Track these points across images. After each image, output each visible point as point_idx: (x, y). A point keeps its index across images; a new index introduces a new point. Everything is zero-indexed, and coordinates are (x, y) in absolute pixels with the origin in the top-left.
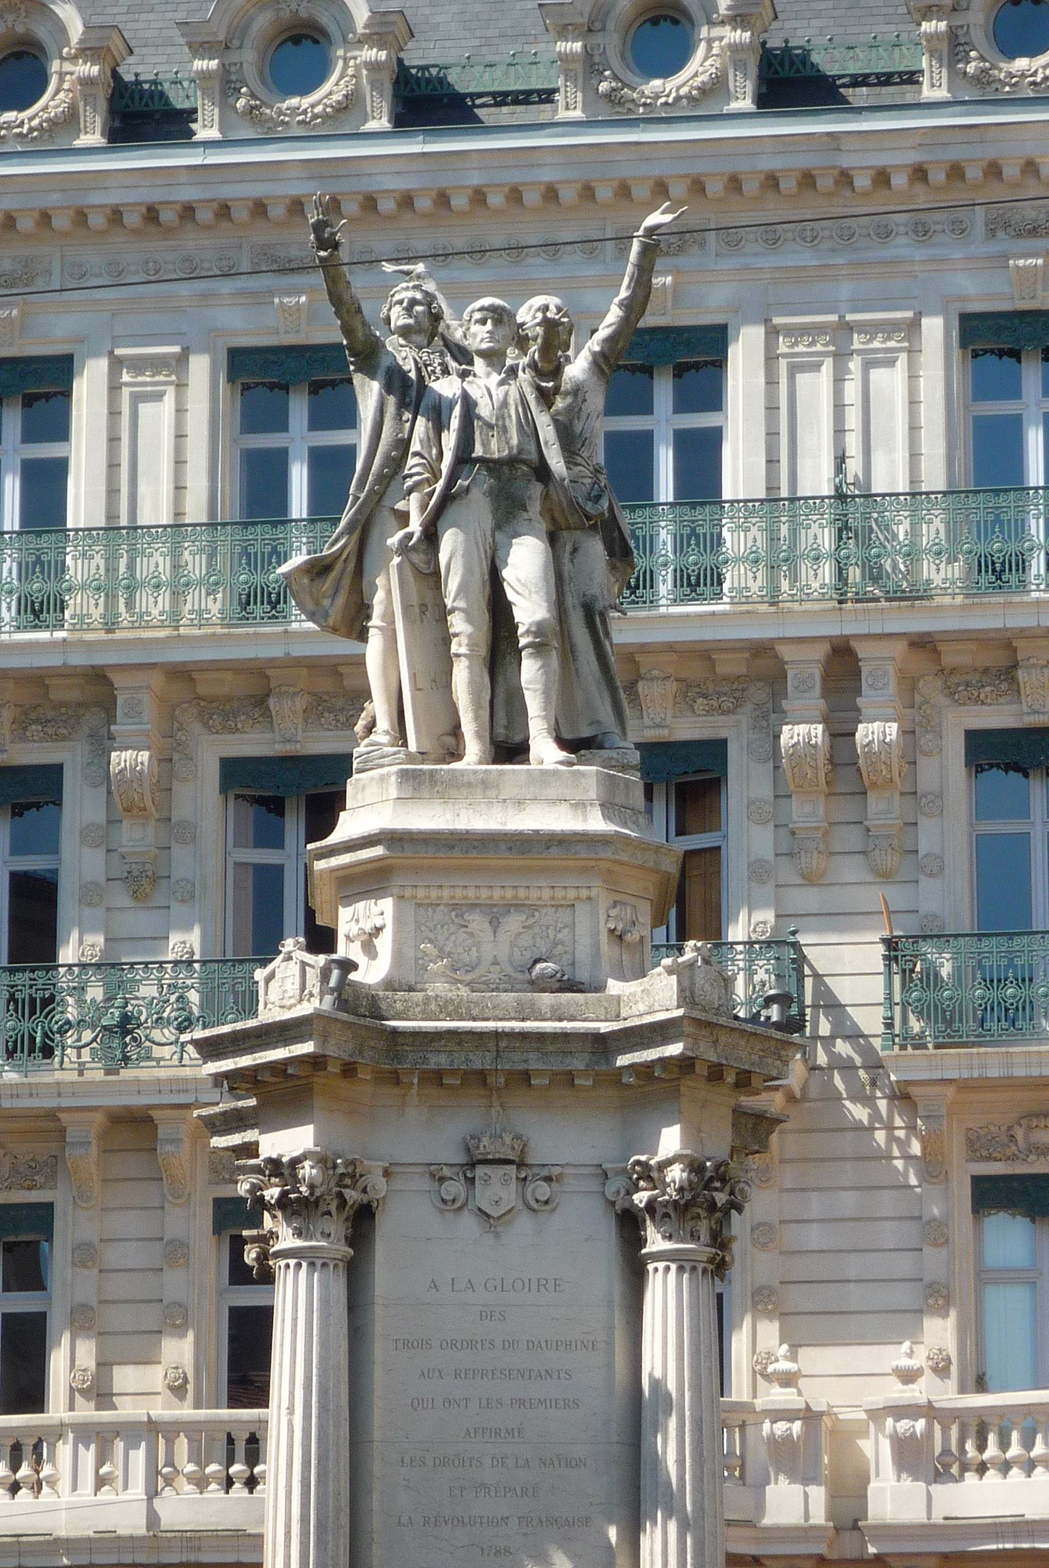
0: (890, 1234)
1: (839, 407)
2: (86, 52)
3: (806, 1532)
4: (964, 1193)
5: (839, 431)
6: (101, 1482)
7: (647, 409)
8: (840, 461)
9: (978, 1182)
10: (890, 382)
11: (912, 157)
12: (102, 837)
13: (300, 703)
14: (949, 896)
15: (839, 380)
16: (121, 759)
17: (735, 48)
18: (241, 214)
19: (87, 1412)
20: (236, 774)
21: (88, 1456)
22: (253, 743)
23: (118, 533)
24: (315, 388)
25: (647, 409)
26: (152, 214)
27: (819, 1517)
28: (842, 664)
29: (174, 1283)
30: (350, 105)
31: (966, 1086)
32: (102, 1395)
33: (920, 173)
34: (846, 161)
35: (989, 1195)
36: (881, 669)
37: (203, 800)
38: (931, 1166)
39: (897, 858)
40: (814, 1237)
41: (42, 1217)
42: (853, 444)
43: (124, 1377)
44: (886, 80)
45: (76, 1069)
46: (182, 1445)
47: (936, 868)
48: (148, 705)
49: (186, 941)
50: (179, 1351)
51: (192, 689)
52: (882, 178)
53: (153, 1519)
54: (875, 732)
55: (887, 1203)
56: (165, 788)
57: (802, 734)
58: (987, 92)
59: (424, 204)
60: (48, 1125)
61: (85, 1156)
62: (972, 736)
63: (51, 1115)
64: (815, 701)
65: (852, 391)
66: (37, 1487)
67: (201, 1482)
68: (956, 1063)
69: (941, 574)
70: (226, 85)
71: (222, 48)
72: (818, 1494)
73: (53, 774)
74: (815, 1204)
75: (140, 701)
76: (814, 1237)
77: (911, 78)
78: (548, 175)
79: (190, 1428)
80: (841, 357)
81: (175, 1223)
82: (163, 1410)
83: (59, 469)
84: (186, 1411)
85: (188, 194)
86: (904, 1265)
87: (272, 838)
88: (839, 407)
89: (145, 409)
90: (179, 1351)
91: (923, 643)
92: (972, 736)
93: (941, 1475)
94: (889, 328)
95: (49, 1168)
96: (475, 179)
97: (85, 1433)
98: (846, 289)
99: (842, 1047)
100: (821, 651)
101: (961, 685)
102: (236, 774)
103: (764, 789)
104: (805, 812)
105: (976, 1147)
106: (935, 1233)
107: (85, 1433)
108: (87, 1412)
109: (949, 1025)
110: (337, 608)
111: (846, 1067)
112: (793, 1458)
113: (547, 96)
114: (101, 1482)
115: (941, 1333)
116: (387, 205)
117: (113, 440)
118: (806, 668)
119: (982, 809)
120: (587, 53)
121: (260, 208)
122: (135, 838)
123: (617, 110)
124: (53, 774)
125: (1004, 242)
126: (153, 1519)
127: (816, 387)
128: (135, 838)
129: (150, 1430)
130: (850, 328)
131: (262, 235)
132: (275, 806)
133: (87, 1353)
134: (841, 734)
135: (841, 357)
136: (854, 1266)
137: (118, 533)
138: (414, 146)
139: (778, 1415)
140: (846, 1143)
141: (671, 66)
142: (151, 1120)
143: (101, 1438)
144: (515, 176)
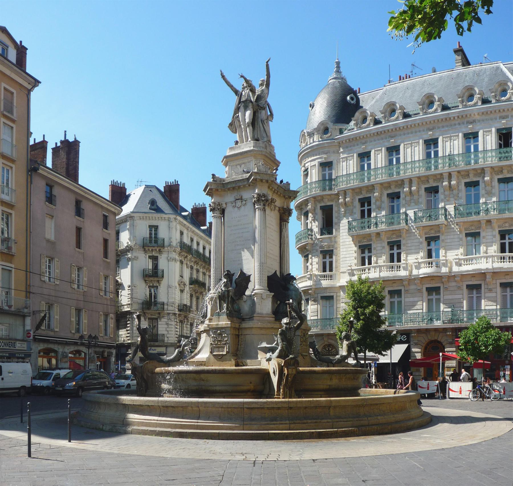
0: (456, 240)
1: (450, 146)
2: (439, 101)
3: (446, 273)
4: (464, 235)
5: (450, 149)
6: (487, 262)
7: (431, 149)
8: (412, 158)
9: (388, 242)
10: (456, 142)
11: (457, 115)
12: (375, 204)
13: (394, 186)
14: (463, 201)
15: (450, 143)
16: (486, 179)
17: (438, 105)
18: (386, 132)
19: (485, 255)
20: (389, 195)
21: (485, 259)
22: (390, 191)
23: (485, 151)
24: (396, 151)
25: (431, 149)
26: (446, 119)
27: (447, 271)
28: (450, 175)
29: (383, 251)
30: (398, 117)
31: (464, 222)
32: (486, 252)
33: (458, 117)
34: (450, 116)
35: (467, 235)
36: (454, 175)
37: (385, 198)
38: (461, 232)
39: (457, 197)
40: (448, 241)
41: (371, 245)
42: (452, 150)
43: (379, 261)
44: (456, 107)
45: (373, 228)
46: (496, 258)
47: (461, 198)
48: (455, 177)
49: (384, 213)
50: (384, 258)
51: (385, 185)
52: (454, 118)
53: (380, 275)
54: (453, 182)
55: (456, 236)
56: (381, 197)
57: (406, 189)
58: (466, 106)
59: (405, 127)
60: (369, 235)
61: (483, 225)
62: (465, 183)
63: (370, 234)
64: (447, 180)
65: (452, 144)
66: (504, 262)
67: (387, 271)
68: (462, 220)
69: (462, 164)
70: (385, 117)
71: (423, 105)
72: (447, 268)
73: (478, 182)
74: (449, 237)
75: (488, 171)
76: (448, 241)
77: (458, 106)
78: (418, 122)
79: (386, 266)
80: (451, 140)
81: (494, 233)
82: (494, 254)
83: (438, 151)
84: (496, 254)
85: (381, 130)
86: (458, 243)
87: (393, 202)
88: (450, 146)
89: (487, 137)
90: (384, 258)
91: (459, 172)
92: (465, 183)
93: (460, 265)
94: (456, 136)
95: (480, 228)
96: (410, 123)
97: (484, 257)
98: (451, 132)
99: (451, 219)
100: (408, 180)
101: (464, 177)
102: (389, 195)
103: (484, 186)
104: (447, 193)
105: (466, 229)
106: (461, 239)
107: (484, 257)
108: (485, 255)
109: (461, 215)
111: (452, 221)
112: (445, 265)
113: (419, 114)
114: (487, 262)
115: (461, 250)
116: (401, 128)
117: (375, 160)
118: (446, 176)
119: (467, 191)
120: (423, 108)
121: (388, 130)
122: (378, 203)
123: (426, 113)
124: (478, 182)
125: (390, 138)
126: (380, 275)
127: (448, 144)
128: (378, 203)
129: (493, 256)
130: (451, 136)
131: (389, 134)
132: (393, 198)
133: (375, 259)
134: (410, 189)
135: (451, 140)
136: (453, 244)
137: (485, 151)
138: (404, 120)
139: (443, 260)
140: (452, 230)
141: (472, 101)
142: (491, 221)
143: (487, 257)
144: (414, 123)
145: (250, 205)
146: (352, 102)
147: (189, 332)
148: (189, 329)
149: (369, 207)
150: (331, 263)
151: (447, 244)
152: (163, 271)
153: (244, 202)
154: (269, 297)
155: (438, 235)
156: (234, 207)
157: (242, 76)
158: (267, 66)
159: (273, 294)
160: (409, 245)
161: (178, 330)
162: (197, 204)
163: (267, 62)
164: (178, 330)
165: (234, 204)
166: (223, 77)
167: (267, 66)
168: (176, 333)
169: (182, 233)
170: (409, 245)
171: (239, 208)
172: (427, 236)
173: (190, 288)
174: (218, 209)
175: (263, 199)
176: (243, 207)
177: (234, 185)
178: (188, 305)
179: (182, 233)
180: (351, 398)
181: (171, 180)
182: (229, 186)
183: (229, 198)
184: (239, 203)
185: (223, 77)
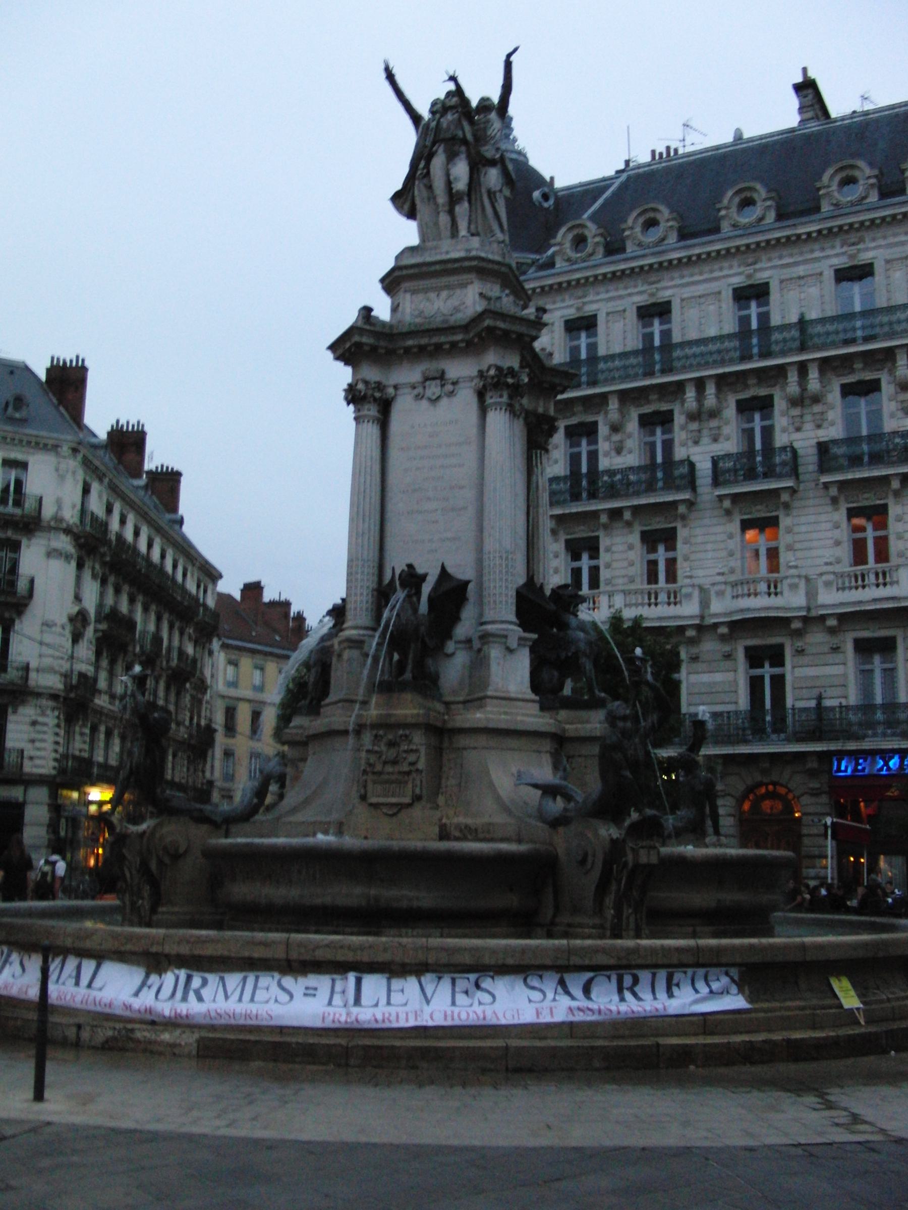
40: (803, 529)
74: (803, 519)
110: (407, 207)
145: (466, 397)
146: (546, 205)
147: (86, 747)
148: (88, 740)
149: (592, 448)
150: (671, 564)
151: (797, 537)
152: (32, 581)
153: (449, 387)
154: (524, 646)
155: (774, 514)
156: (419, 397)
157: (453, 78)
158: (508, 65)
159: (535, 636)
160: (699, 539)
161: (61, 740)
162: (123, 422)
163: (509, 56)
164: (61, 740)
165: (420, 390)
166: (390, 77)
167: (508, 65)
168: (57, 747)
169: (86, 491)
170: (699, 539)
171: (434, 401)
172: (746, 517)
173: (96, 631)
174: (375, 400)
175: (510, 381)
176: (444, 401)
177: (424, 341)
178: (89, 674)
179: (86, 491)
180: (737, 941)
181: (67, 355)
182: (410, 343)
183: (407, 374)
184: (433, 389)
185: (390, 77)
